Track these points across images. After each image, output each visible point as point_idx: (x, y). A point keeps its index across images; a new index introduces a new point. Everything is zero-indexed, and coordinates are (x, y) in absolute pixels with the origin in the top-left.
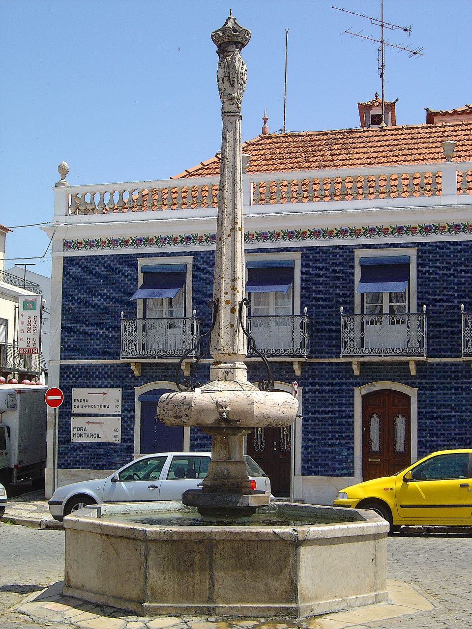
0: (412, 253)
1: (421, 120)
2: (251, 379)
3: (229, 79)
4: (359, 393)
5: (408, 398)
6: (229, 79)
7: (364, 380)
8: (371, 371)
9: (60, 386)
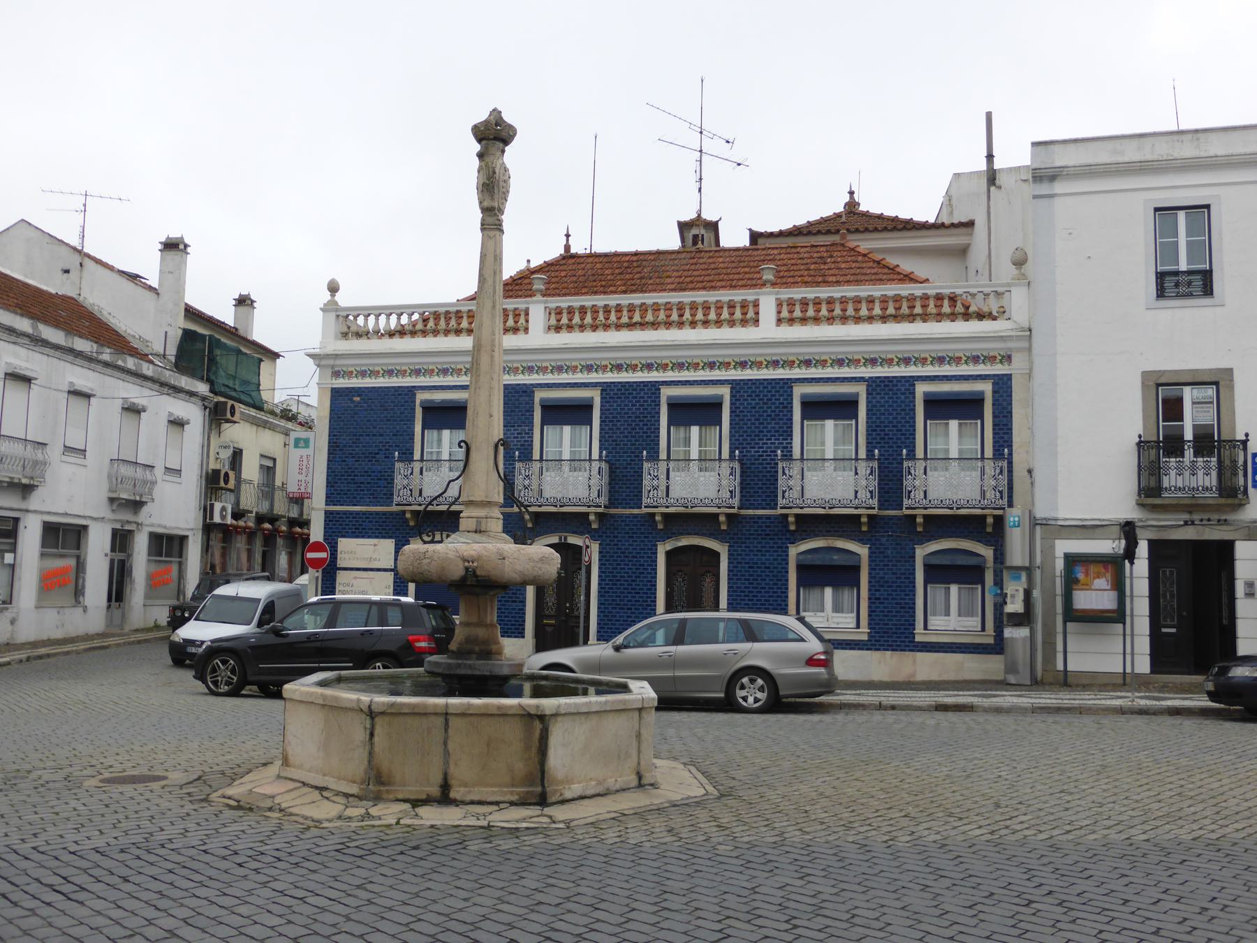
0: (725, 392)
1: (744, 241)
2: (506, 530)
3: (492, 189)
4: (662, 550)
5: (717, 555)
6: (492, 189)
7: (667, 535)
8: (942, 524)
9: (325, 539)
